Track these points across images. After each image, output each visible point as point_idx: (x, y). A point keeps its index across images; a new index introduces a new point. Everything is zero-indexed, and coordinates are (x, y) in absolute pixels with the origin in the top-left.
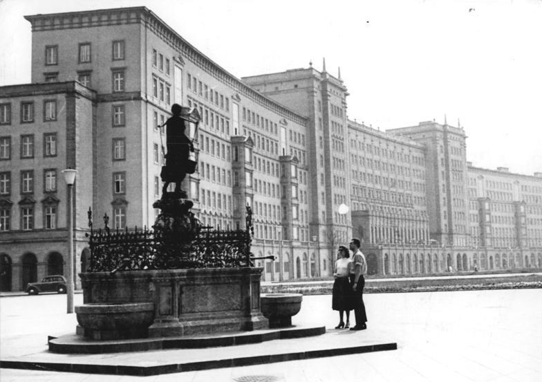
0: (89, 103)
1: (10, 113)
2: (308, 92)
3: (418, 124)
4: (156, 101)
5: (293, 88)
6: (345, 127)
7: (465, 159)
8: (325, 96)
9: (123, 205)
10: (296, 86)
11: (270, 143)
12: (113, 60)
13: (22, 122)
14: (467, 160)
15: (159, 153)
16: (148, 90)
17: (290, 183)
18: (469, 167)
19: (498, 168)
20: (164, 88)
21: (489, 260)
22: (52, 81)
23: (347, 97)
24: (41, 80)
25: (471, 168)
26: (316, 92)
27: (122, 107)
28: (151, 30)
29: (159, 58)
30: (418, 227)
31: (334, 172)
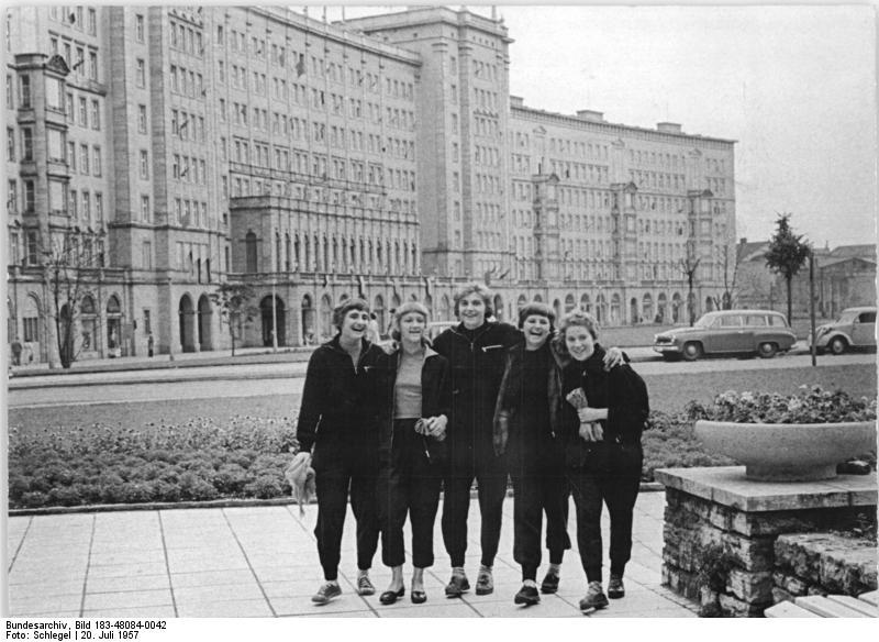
5: (412, 38)
7: (507, 91)
14: (513, 92)
17: (41, 124)
18: (513, 108)
19: (579, 112)
21: (629, 306)
23: (510, 45)
25: (519, 110)
30: (313, 228)
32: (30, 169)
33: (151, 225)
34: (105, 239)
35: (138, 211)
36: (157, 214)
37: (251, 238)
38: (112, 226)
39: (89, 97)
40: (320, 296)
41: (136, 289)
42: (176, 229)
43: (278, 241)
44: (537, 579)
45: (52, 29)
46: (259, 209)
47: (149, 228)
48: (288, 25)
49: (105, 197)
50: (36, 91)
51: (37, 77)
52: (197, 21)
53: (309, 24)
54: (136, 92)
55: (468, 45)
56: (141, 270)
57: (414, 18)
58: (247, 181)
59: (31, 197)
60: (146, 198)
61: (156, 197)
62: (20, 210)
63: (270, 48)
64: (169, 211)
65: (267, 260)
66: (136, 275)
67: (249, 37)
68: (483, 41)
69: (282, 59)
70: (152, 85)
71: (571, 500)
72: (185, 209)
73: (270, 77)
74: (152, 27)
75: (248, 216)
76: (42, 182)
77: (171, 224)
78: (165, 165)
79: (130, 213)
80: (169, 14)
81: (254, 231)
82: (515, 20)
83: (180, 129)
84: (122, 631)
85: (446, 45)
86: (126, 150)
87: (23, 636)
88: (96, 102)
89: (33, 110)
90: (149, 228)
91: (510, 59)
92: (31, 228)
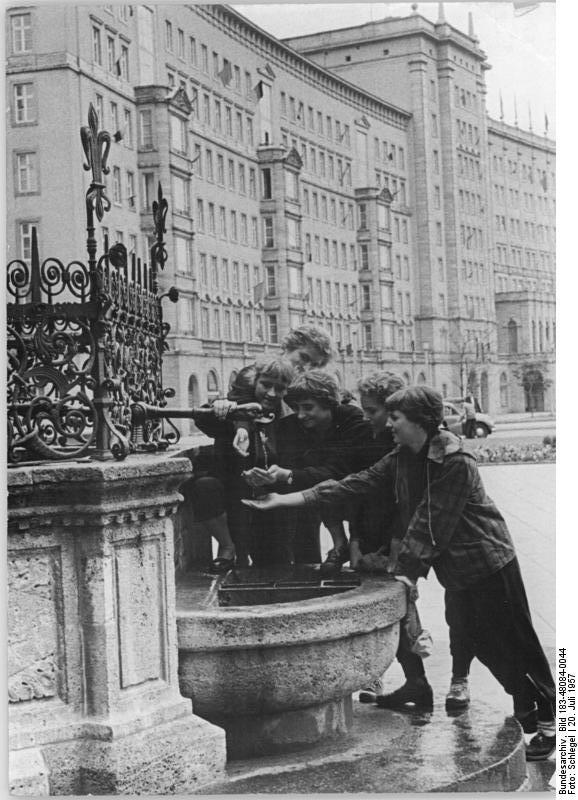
17: (375, 242)
18: (489, 132)
32: (367, 276)
33: (446, 317)
34: (413, 328)
35: (438, 307)
36: (450, 309)
37: (512, 325)
38: (417, 319)
39: (401, 217)
40: (417, 374)
41: (437, 366)
42: (464, 320)
43: (534, 327)
45: (377, 167)
46: (518, 301)
47: (444, 319)
48: (534, 147)
49: (412, 296)
50: (370, 218)
51: (371, 205)
52: (476, 152)
53: (535, 140)
54: (435, 214)
55: (450, 64)
56: (440, 353)
57: (382, 31)
58: (506, 279)
59: (367, 298)
60: (442, 296)
61: (449, 295)
62: (359, 308)
63: (521, 168)
64: (460, 306)
65: (525, 343)
66: (437, 356)
67: (506, 159)
68: (464, 62)
69: (530, 177)
70: (445, 206)
72: (470, 303)
73: (521, 192)
74: (444, 160)
75: (511, 308)
76: (375, 287)
77: (462, 316)
78: (456, 269)
79: (432, 309)
80: (457, 149)
81: (515, 319)
82: (492, 29)
83: (467, 241)
84: (568, 689)
85: (425, 63)
86: (428, 258)
88: (405, 222)
89: (368, 231)
90: (444, 319)
92: (368, 321)
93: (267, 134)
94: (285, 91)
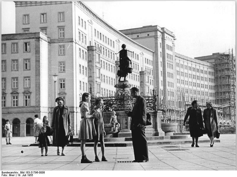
0: (47, 43)
1: (17, 47)
2: (155, 38)
3: (212, 54)
4: (80, 43)
6: (174, 56)
8: (163, 39)
9: (64, 95)
10: (148, 35)
11: (135, 65)
12: (59, 22)
13: (59, 55)
15: (105, 65)
16: (76, 37)
20: (82, 36)
22: (27, 32)
24: (21, 32)
26: (159, 38)
27: (64, 46)
28: (77, 6)
29: (81, 21)
31: (168, 79)
44: (41, 118)
71: (189, 116)
87: (6, 175)
91: (179, 53)
93: (90, 42)
94: (107, 37)
